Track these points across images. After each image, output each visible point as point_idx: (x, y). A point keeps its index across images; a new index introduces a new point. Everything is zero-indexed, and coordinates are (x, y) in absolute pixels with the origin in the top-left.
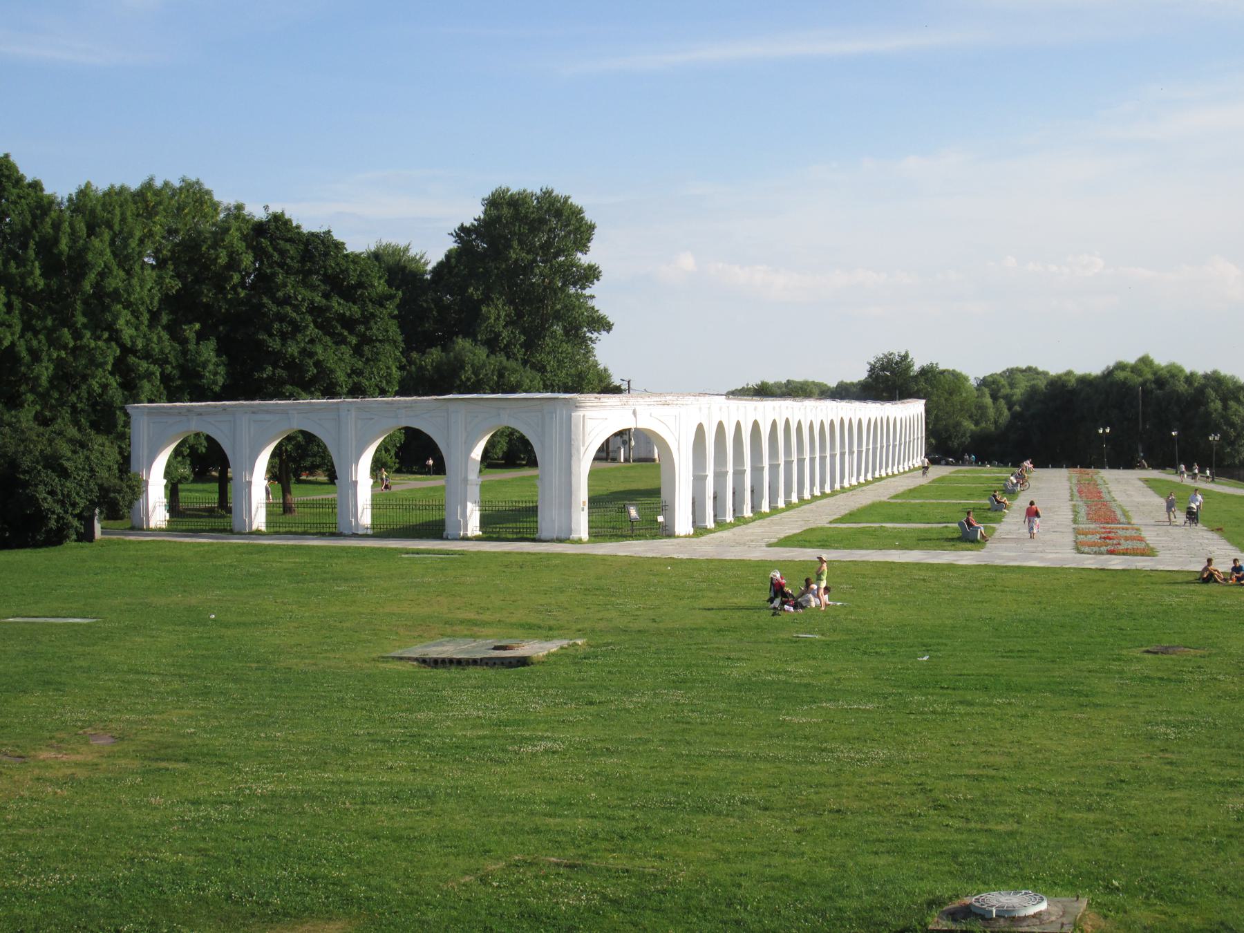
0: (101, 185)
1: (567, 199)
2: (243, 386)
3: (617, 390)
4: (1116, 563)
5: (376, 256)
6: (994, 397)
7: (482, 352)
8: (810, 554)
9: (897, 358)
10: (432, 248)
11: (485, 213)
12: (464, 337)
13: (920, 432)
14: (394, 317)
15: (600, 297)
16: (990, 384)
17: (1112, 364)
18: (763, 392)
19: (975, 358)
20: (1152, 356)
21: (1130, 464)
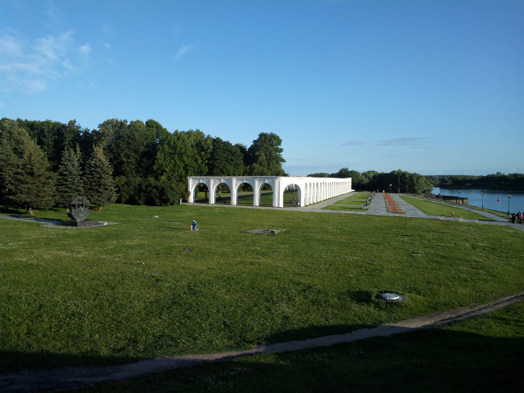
0: (180, 131)
2: (211, 173)
3: (286, 175)
4: (397, 215)
5: (237, 145)
6: (366, 177)
8: (330, 211)
10: (248, 144)
13: (350, 185)
15: (283, 155)
16: (365, 174)
18: (322, 175)
19: (361, 168)
21: (397, 192)
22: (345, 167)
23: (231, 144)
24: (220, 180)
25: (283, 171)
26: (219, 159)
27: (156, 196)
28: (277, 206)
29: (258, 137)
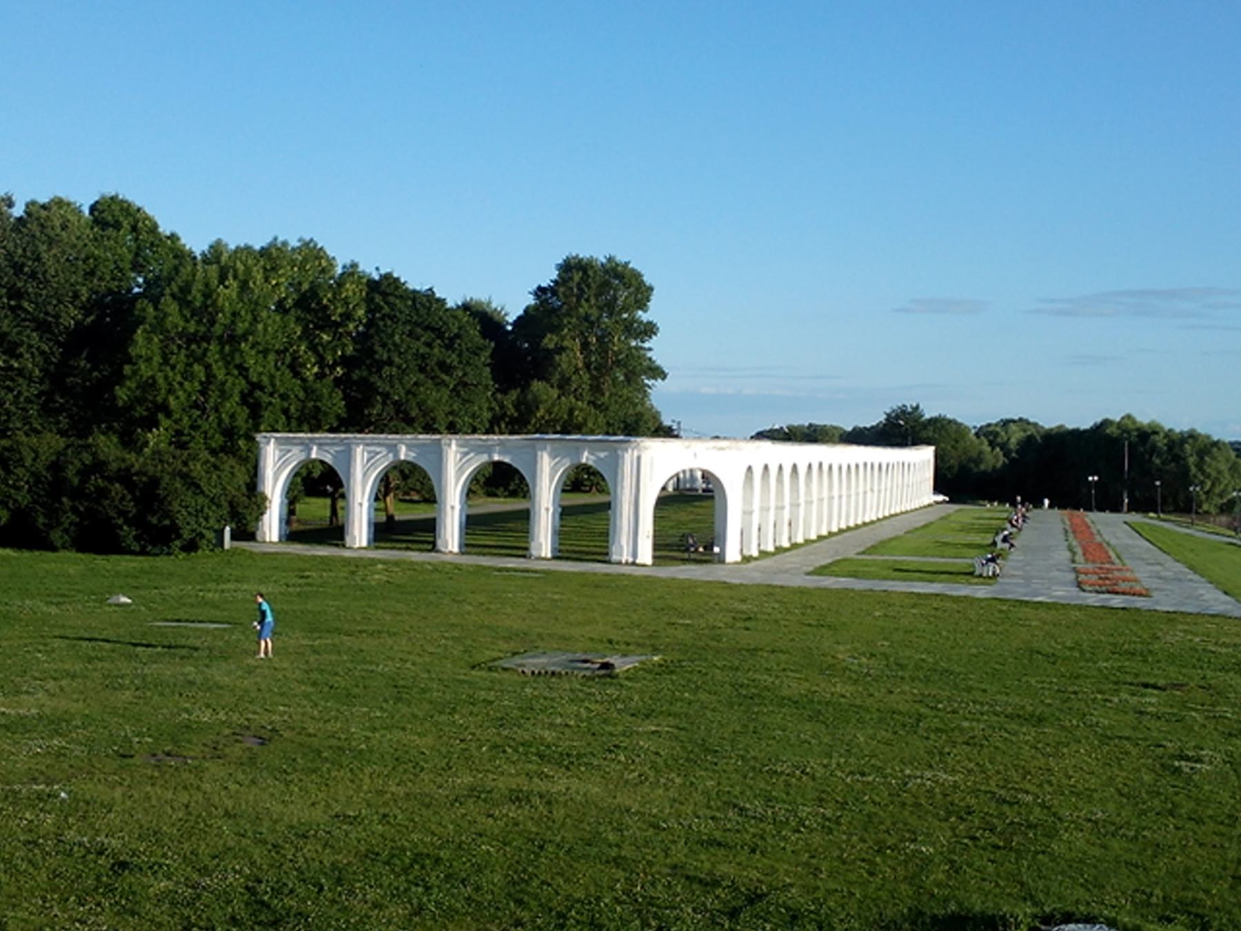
1: (627, 263)
2: (356, 419)
4: (1117, 601)
5: (466, 307)
7: (555, 393)
9: (909, 410)
10: (512, 303)
11: (559, 275)
12: (539, 380)
13: (928, 475)
14: (488, 365)
16: (988, 433)
17: (1099, 420)
19: (974, 409)
20: (584, 252)
21: (1116, 509)
22: (910, 404)
23: (442, 302)
24: (393, 448)
25: (656, 416)
26: (390, 363)
27: (123, 513)
28: (626, 557)
29: (554, 275)
